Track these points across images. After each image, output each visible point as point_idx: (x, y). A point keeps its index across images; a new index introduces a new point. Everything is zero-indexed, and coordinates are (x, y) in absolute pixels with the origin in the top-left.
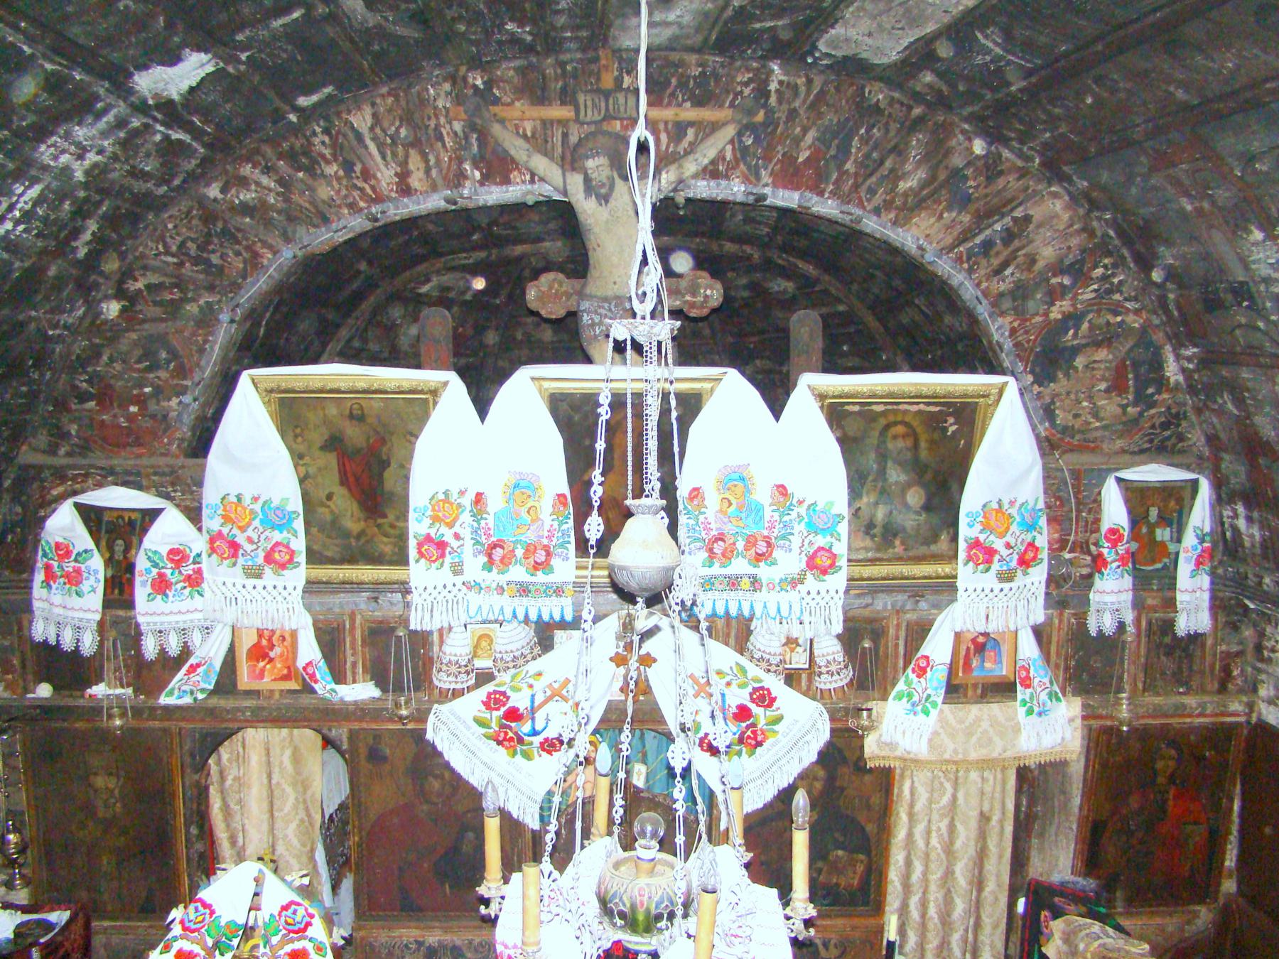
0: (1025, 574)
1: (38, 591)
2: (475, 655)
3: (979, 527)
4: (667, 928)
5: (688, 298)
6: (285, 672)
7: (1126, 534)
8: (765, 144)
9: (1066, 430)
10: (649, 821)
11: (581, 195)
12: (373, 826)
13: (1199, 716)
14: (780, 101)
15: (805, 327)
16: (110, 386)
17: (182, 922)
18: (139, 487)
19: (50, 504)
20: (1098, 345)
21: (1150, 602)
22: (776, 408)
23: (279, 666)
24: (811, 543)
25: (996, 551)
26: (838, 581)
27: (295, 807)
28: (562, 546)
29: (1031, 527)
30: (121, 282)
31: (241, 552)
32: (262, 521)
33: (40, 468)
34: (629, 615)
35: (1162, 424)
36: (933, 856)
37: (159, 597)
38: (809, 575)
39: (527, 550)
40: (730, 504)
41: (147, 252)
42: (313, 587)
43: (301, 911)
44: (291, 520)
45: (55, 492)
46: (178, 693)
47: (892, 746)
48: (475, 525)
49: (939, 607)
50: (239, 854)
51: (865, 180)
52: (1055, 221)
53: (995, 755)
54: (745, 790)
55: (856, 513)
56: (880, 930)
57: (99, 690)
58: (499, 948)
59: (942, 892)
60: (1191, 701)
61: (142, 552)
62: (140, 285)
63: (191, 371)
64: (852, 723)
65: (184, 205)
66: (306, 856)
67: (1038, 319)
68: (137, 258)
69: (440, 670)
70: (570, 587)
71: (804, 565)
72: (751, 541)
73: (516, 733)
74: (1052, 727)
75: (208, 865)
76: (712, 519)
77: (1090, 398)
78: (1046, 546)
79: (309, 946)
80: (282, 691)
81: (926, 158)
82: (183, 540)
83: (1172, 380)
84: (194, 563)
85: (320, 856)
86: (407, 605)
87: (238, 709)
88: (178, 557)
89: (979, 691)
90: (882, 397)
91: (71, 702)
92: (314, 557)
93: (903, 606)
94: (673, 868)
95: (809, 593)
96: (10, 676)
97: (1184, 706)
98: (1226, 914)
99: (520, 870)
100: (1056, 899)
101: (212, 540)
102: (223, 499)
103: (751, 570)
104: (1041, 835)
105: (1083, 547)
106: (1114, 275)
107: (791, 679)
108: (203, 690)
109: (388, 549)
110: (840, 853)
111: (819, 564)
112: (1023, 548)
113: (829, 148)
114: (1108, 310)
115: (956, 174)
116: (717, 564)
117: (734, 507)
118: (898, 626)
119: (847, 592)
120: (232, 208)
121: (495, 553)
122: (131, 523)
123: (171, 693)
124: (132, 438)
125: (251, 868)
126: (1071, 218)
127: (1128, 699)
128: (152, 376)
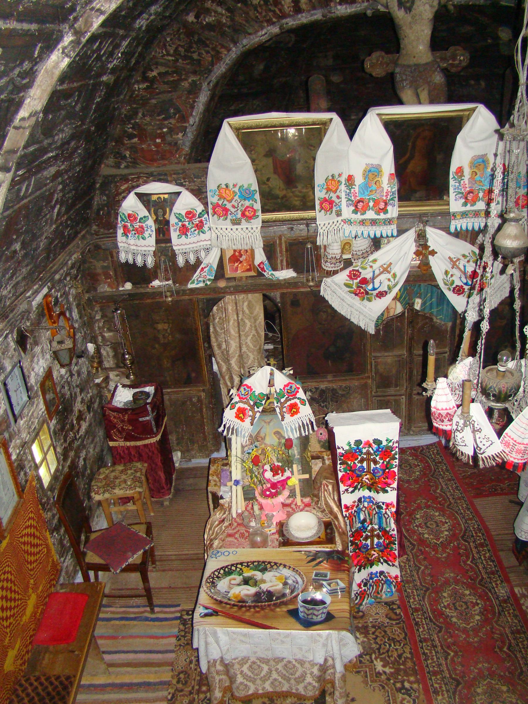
2: (342, 253)
5: (451, 62)
6: (248, 267)
11: (396, 8)
16: (145, 129)
18: (166, 181)
27: (251, 329)
28: (392, 199)
30: (144, 73)
32: (239, 197)
33: (114, 176)
37: (184, 236)
41: (157, 55)
45: (123, 188)
46: (197, 282)
48: (348, 191)
57: (156, 283)
62: (154, 73)
63: (188, 118)
65: (175, 27)
68: (151, 59)
73: (365, 290)
79: (298, 401)
82: (192, 206)
84: (199, 217)
91: (142, 290)
102: (218, 187)
109: (297, 203)
116: (469, 205)
120: (203, 27)
121: (359, 205)
123: (193, 283)
124: (164, 156)
128: (166, 122)
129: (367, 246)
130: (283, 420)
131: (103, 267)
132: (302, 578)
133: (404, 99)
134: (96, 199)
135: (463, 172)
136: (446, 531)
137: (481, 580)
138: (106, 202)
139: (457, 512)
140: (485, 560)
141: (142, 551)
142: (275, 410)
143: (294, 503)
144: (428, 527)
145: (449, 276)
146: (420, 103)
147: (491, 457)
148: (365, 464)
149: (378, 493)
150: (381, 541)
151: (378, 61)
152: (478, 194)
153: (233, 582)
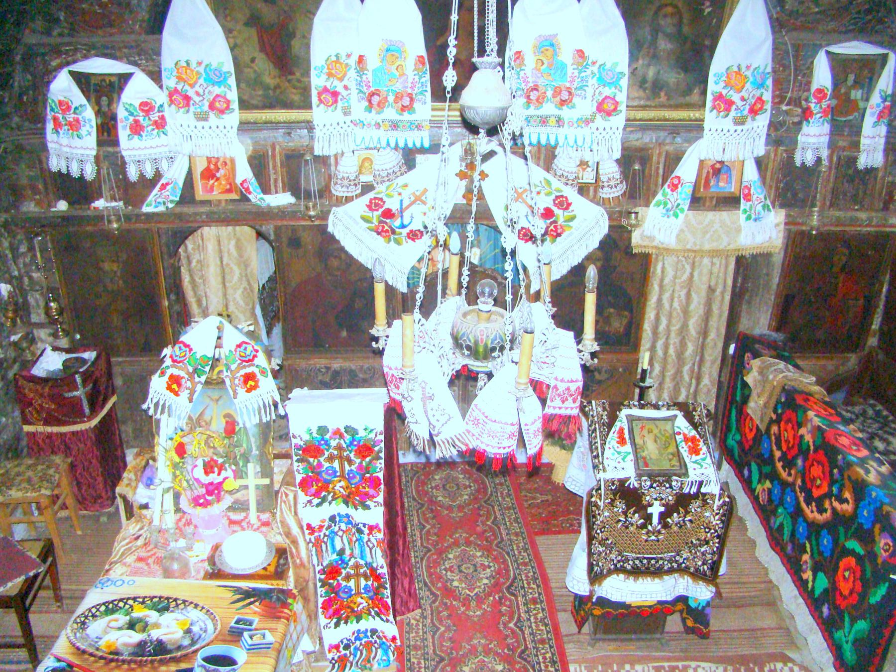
0: (753, 119)
1: (50, 136)
2: (360, 172)
3: (722, 84)
4: (499, 357)
6: (228, 187)
7: (829, 93)
9: (791, 13)
10: (486, 286)
12: (294, 291)
13: (867, 226)
17: (171, 357)
18: (115, 58)
19: (49, 75)
21: (841, 143)
23: (223, 183)
24: (600, 93)
26: (619, 121)
27: (240, 280)
28: (422, 93)
29: (761, 85)
31: (192, 102)
32: (205, 80)
34: (469, 143)
36: (674, 314)
37: (136, 137)
39: (396, 97)
40: (543, 64)
42: (245, 127)
43: (250, 348)
44: (225, 79)
45: (54, 64)
46: (155, 203)
47: (651, 238)
48: (359, 79)
49: (691, 142)
50: (204, 311)
53: (721, 247)
54: (553, 264)
55: (633, 72)
56: (636, 362)
57: (100, 204)
58: (386, 370)
59: (680, 338)
60: (863, 215)
61: (121, 105)
64: (624, 222)
66: (250, 318)
69: (336, 184)
70: (428, 123)
71: (594, 109)
72: (557, 91)
73: (390, 227)
74: (762, 229)
75: (184, 319)
76: (529, 74)
78: (770, 99)
79: (257, 371)
80: (226, 200)
84: (159, 111)
85: (258, 311)
86: (312, 138)
87: (196, 214)
88: (147, 107)
89: (714, 202)
92: (244, 105)
93: (664, 140)
94: (502, 316)
95: (597, 129)
96: (38, 197)
97: (857, 219)
98: (867, 362)
99: (400, 318)
100: (757, 346)
101: (171, 95)
102: (176, 64)
103: (557, 112)
104: (749, 302)
105: (796, 102)
107: (583, 190)
108: (172, 201)
109: (296, 98)
110: (612, 310)
111: (606, 108)
112: (753, 101)
116: (532, 107)
117: (545, 66)
118: (660, 154)
119: (624, 129)
121: (373, 99)
122: (111, 84)
123: (150, 205)
125: (213, 321)
127: (818, 212)
129: (395, 163)
130: (235, 397)
131: (30, 178)
132: (215, 625)
134: (17, 79)
135: (523, 59)
136: (487, 578)
137: (523, 652)
138: (31, 83)
139: (508, 554)
140: (535, 622)
141: (23, 578)
142: (223, 382)
143: (247, 520)
144: (461, 571)
147: (450, 441)
148: (336, 464)
149: (356, 509)
150: (370, 583)
153: (113, 624)
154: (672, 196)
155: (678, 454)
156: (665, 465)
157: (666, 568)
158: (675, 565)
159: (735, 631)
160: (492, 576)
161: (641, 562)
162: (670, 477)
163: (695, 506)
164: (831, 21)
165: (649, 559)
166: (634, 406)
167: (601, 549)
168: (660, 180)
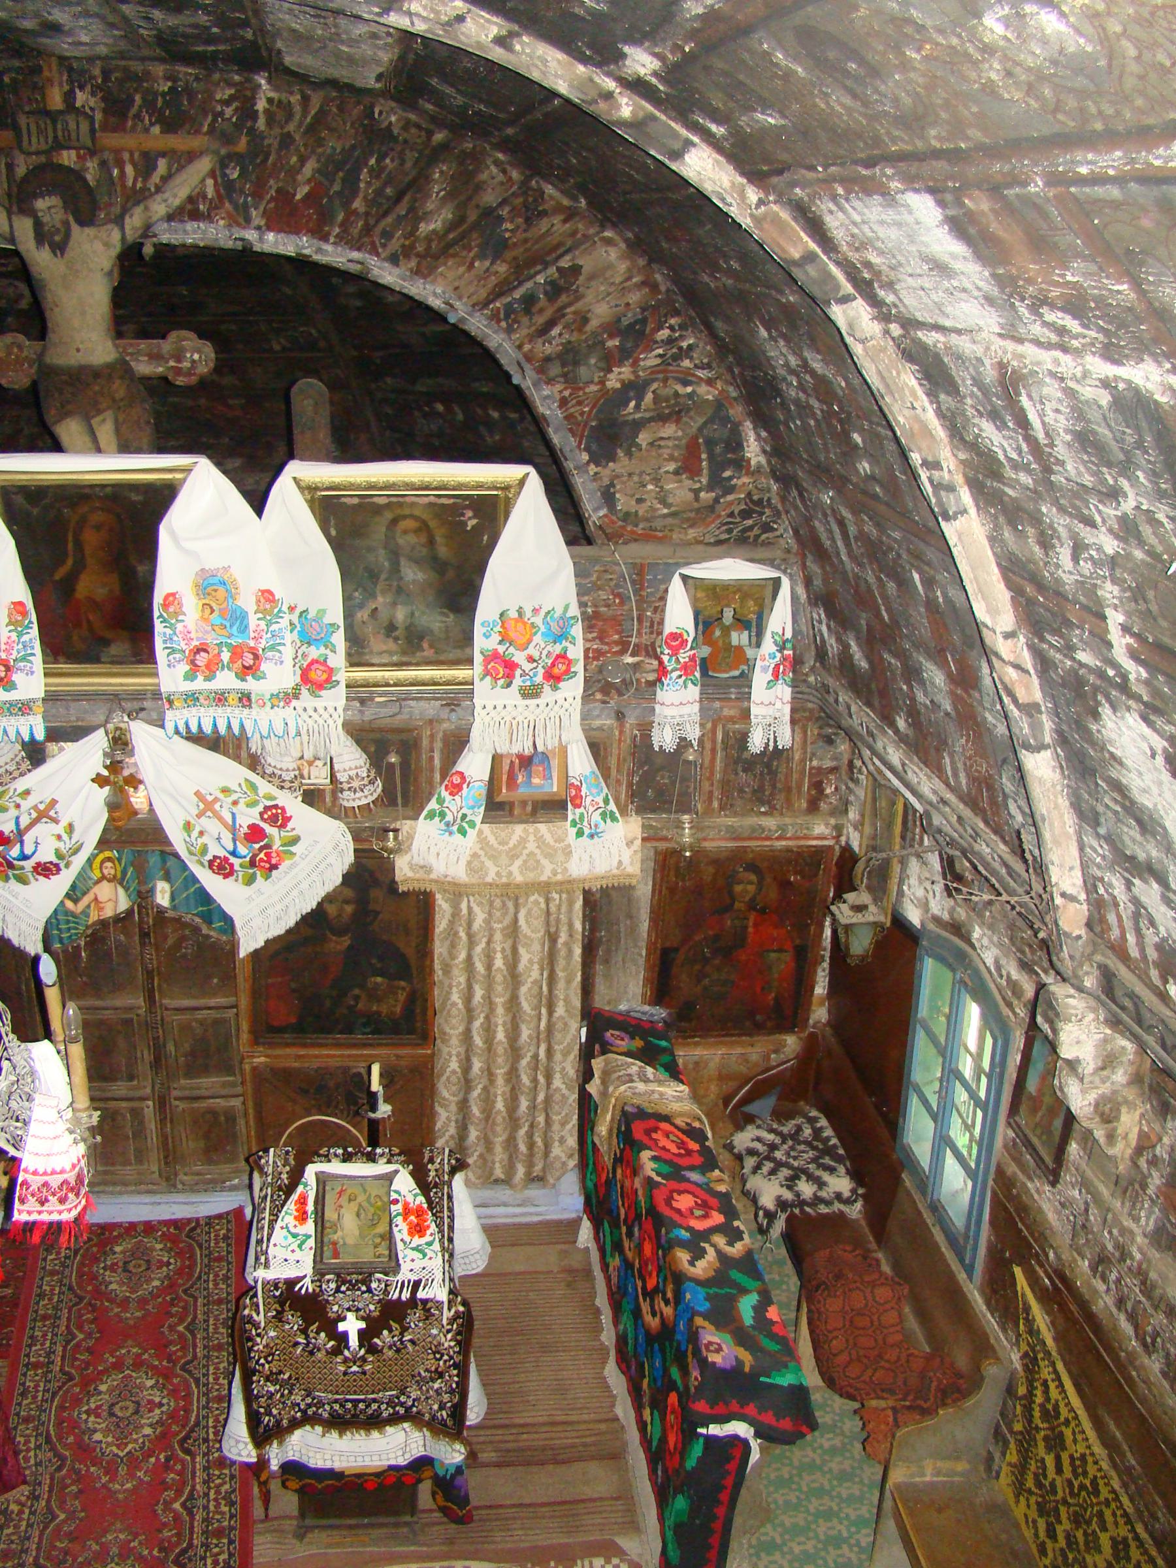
0: (555, 688)
5: (172, 363)
7: (690, 639)
8: (253, 177)
9: (627, 516)
13: (779, 838)
14: (270, 122)
15: (310, 399)
20: (662, 419)
21: (727, 712)
22: (258, 503)
25: (517, 665)
35: (742, 512)
38: (305, 692)
40: (213, 611)
47: (427, 869)
51: (377, 222)
52: (608, 274)
53: (544, 878)
60: (770, 823)
67: (593, 388)
71: (298, 680)
74: (609, 847)
76: (191, 626)
77: (656, 481)
81: (451, 195)
83: (753, 463)
89: (529, 808)
90: (381, 489)
98: (811, 1045)
102: (502, 615)
103: (238, 685)
104: (606, 961)
106: (682, 337)
107: (312, 797)
110: (379, 979)
111: (313, 678)
112: (550, 662)
113: (332, 182)
114: (676, 379)
115: (489, 215)
116: (200, 678)
118: (432, 736)
126: (629, 269)
133: (65, 439)
136: (151, 1425)
139: (197, 1381)
140: (216, 1500)
144: (112, 1414)
145: (195, 834)
146: (99, 450)
151: (9, 354)
152: (219, 654)
154: (453, 804)
155: (389, 1237)
156: (367, 1256)
157: (385, 1414)
158: (402, 1411)
159: (543, 1505)
160: (160, 1422)
161: (342, 1406)
162: (371, 1274)
163: (414, 1318)
164: (691, 526)
165: (355, 1402)
166: (336, 1155)
167: (272, 1389)
168: (437, 776)
